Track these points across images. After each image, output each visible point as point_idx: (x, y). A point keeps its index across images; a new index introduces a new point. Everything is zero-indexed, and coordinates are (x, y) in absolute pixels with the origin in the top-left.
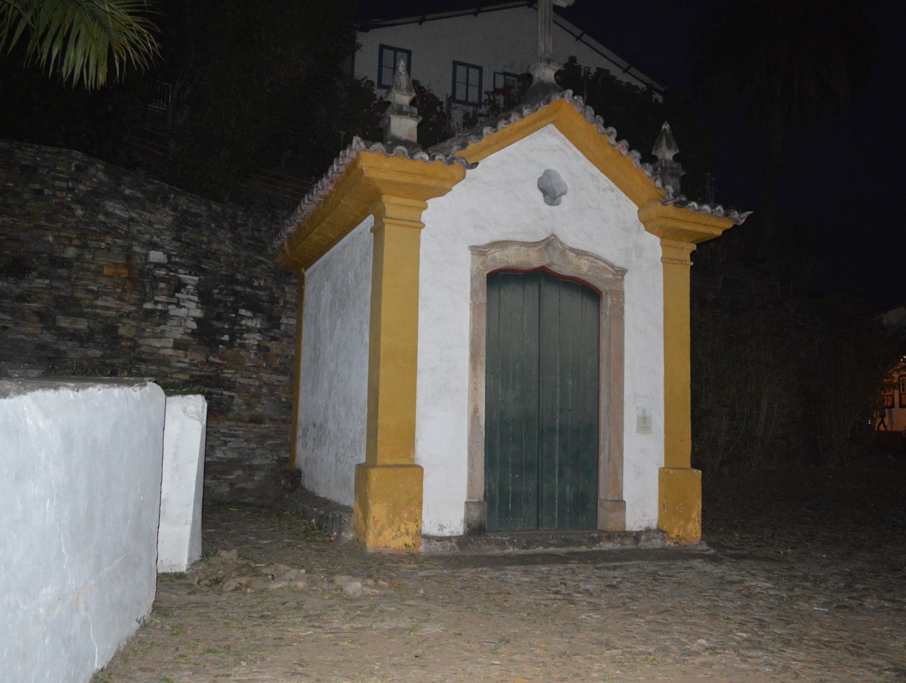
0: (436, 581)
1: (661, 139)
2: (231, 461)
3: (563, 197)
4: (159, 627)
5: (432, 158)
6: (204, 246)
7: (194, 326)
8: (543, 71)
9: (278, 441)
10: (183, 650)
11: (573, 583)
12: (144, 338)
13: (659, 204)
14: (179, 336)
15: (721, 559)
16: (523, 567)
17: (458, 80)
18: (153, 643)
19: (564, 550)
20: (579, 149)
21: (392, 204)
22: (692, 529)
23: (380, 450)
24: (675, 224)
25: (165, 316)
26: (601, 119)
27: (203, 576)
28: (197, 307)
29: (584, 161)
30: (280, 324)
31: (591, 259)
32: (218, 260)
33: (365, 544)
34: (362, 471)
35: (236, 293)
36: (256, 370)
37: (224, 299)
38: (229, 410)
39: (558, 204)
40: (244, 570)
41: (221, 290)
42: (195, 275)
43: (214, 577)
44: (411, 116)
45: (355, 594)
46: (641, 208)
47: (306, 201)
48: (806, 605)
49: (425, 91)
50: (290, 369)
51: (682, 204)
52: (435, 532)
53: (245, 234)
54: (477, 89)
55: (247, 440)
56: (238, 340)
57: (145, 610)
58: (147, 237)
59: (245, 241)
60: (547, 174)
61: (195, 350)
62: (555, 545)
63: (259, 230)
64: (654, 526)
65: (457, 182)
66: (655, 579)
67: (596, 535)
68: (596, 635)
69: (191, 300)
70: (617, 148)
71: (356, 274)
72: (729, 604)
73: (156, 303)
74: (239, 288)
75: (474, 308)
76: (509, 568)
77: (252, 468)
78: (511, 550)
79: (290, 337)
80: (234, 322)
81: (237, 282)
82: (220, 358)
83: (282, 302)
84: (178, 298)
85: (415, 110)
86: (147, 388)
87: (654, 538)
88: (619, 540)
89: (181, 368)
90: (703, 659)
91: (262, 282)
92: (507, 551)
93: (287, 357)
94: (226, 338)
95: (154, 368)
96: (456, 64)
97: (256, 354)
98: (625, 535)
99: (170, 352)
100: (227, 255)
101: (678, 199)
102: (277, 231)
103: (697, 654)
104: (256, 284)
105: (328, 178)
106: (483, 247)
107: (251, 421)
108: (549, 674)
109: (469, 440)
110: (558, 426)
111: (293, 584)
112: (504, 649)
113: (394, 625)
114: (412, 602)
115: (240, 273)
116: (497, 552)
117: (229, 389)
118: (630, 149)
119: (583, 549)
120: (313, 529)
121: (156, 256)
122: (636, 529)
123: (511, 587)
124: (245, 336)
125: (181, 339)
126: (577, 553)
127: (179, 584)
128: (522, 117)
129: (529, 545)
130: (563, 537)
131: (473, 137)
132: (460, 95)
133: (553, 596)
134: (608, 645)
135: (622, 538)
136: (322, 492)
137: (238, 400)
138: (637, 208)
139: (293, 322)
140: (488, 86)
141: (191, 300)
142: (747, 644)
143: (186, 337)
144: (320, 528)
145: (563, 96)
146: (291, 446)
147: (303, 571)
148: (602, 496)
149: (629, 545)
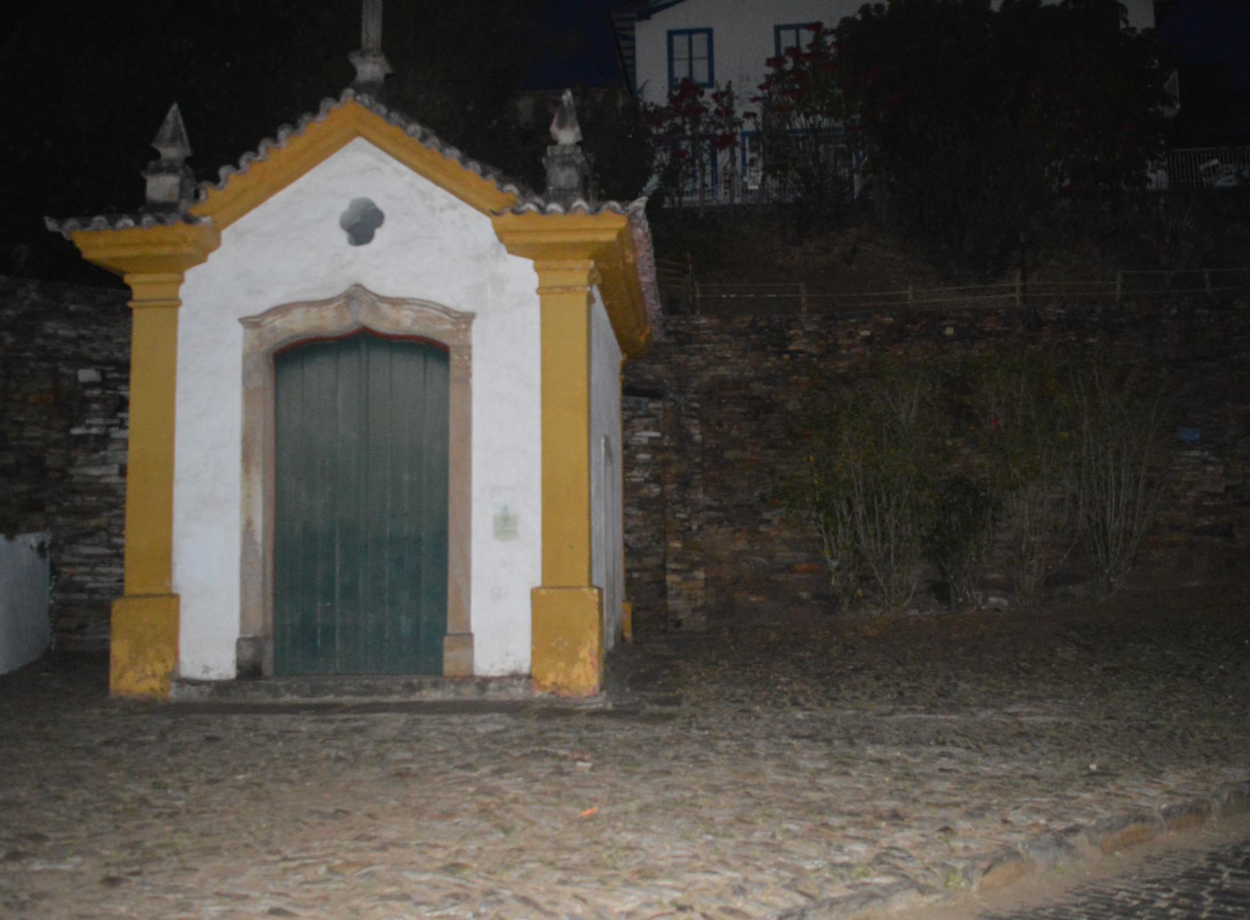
17: (676, 55)
22: (583, 676)
31: (416, 308)
52: (198, 674)
62: (351, 693)
78: (288, 698)
87: (512, 685)
106: (259, 316)
116: (268, 699)
129: (314, 691)
135: (458, 684)
149: (469, 693)
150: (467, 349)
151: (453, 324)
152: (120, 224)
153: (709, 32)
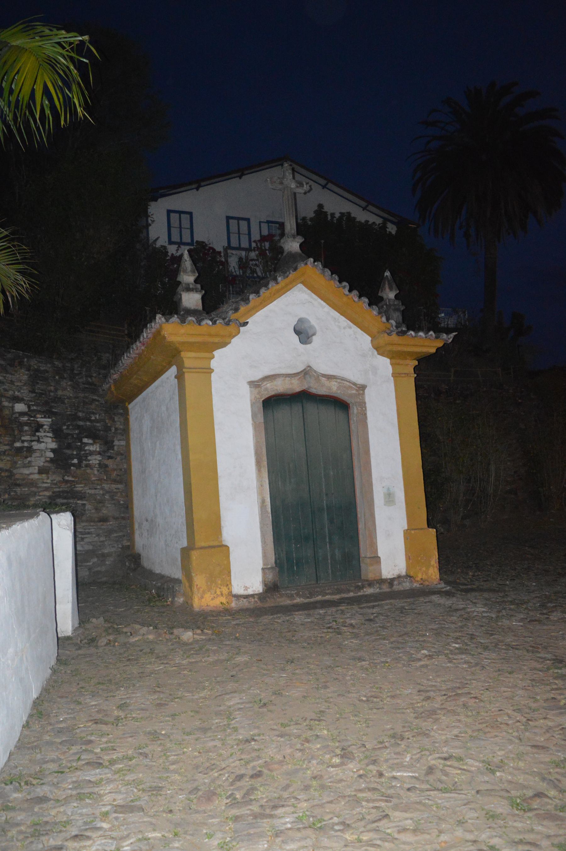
0: (244, 627)
1: (384, 284)
2: (87, 552)
3: (314, 337)
4: (63, 672)
5: (214, 323)
6: (52, 394)
7: (51, 455)
8: (290, 244)
9: (120, 534)
10: (82, 684)
11: (342, 620)
12: (17, 468)
13: (386, 335)
14: (42, 464)
15: (454, 593)
16: (306, 612)
18: (62, 681)
19: (337, 597)
20: (322, 299)
21: (189, 358)
23: (197, 537)
24: (400, 348)
25: (30, 450)
26: (337, 278)
27: (83, 637)
28: (53, 441)
29: (327, 308)
30: (114, 446)
32: (63, 403)
33: (192, 605)
34: (186, 553)
35: (79, 427)
36: (99, 482)
37: (71, 433)
38: (83, 515)
39: (310, 343)
40: (110, 631)
41: (68, 426)
42: (49, 418)
43: (90, 637)
44: (197, 291)
45: (188, 640)
46: (373, 338)
47: (126, 358)
48: (508, 622)
49: (206, 245)
50: (124, 479)
51: (403, 333)
52: (242, 592)
53: (80, 380)
54: (247, 236)
55: (98, 535)
56: (84, 462)
57: (53, 662)
58: (11, 393)
59: (82, 386)
60: (301, 321)
61: (54, 473)
63: (91, 377)
64: (404, 573)
65: (234, 336)
66: (402, 613)
67: (360, 584)
68: (353, 654)
69: (47, 437)
70: (350, 297)
71: (167, 409)
72: (453, 626)
73: (23, 442)
74: (81, 423)
75: (256, 427)
76: (297, 613)
77: (103, 555)
78: (298, 600)
79: (122, 454)
80: (80, 449)
81: (80, 419)
82: (73, 477)
83: (113, 429)
84: (38, 436)
85: (199, 286)
86: (40, 517)
87: (404, 582)
88: (378, 585)
89: (46, 487)
90: (422, 663)
91: (97, 416)
92: (295, 601)
93: (121, 470)
94: (75, 461)
95: (26, 489)
96: (228, 218)
97: (98, 471)
98: (382, 581)
99: (36, 476)
100: (69, 398)
101: (400, 329)
102: (105, 377)
103: (420, 660)
104: (93, 418)
105: (140, 342)
106: (257, 381)
107: (100, 521)
108: (318, 680)
109: (260, 523)
110: (325, 507)
111: (146, 637)
112: (289, 667)
113: (216, 658)
114: (228, 643)
115: (80, 411)
116: (288, 602)
117: (81, 498)
118: (360, 297)
119: (351, 594)
120: (154, 597)
121: (20, 407)
122: (390, 576)
123: (297, 627)
124: (89, 458)
125: (43, 466)
126: (347, 598)
127: (68, 644)
128: (277, 283)
129: (311, 595)
130: (336, 587)
131: (242, 303)
132: (234, 243)
133: (325, 631)
134: (360, 659)
136: (157, 570)
137: (88, 507)
138: (370, 339)
139: (123, 443)
140: (256, 236)
141: (47, 437)
142: (457, 651)
143: (46, 464)
144: (159, 596)
145: (306, 264)
146: (131, 536)
147: (151, 628)
148: (362, 555)
149: (386, 588)
150: (363, 405)
151: (357, 390)
152: (204, 323)
153: (191, 214)
